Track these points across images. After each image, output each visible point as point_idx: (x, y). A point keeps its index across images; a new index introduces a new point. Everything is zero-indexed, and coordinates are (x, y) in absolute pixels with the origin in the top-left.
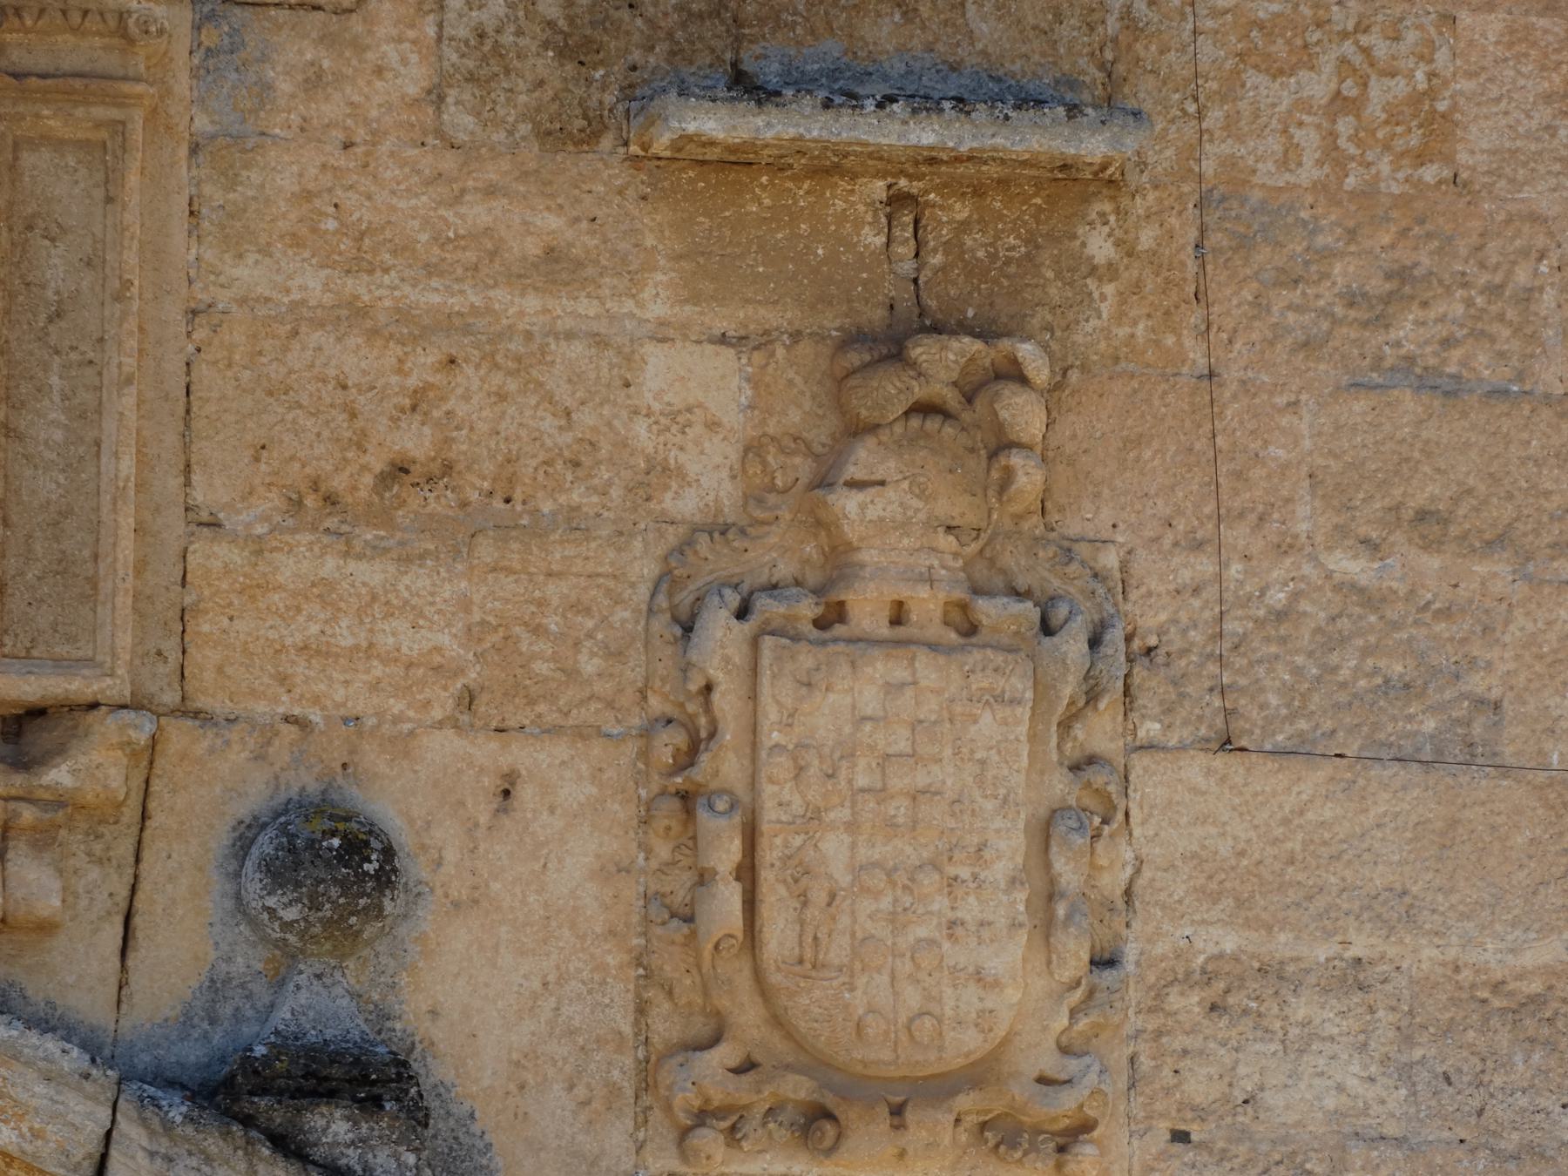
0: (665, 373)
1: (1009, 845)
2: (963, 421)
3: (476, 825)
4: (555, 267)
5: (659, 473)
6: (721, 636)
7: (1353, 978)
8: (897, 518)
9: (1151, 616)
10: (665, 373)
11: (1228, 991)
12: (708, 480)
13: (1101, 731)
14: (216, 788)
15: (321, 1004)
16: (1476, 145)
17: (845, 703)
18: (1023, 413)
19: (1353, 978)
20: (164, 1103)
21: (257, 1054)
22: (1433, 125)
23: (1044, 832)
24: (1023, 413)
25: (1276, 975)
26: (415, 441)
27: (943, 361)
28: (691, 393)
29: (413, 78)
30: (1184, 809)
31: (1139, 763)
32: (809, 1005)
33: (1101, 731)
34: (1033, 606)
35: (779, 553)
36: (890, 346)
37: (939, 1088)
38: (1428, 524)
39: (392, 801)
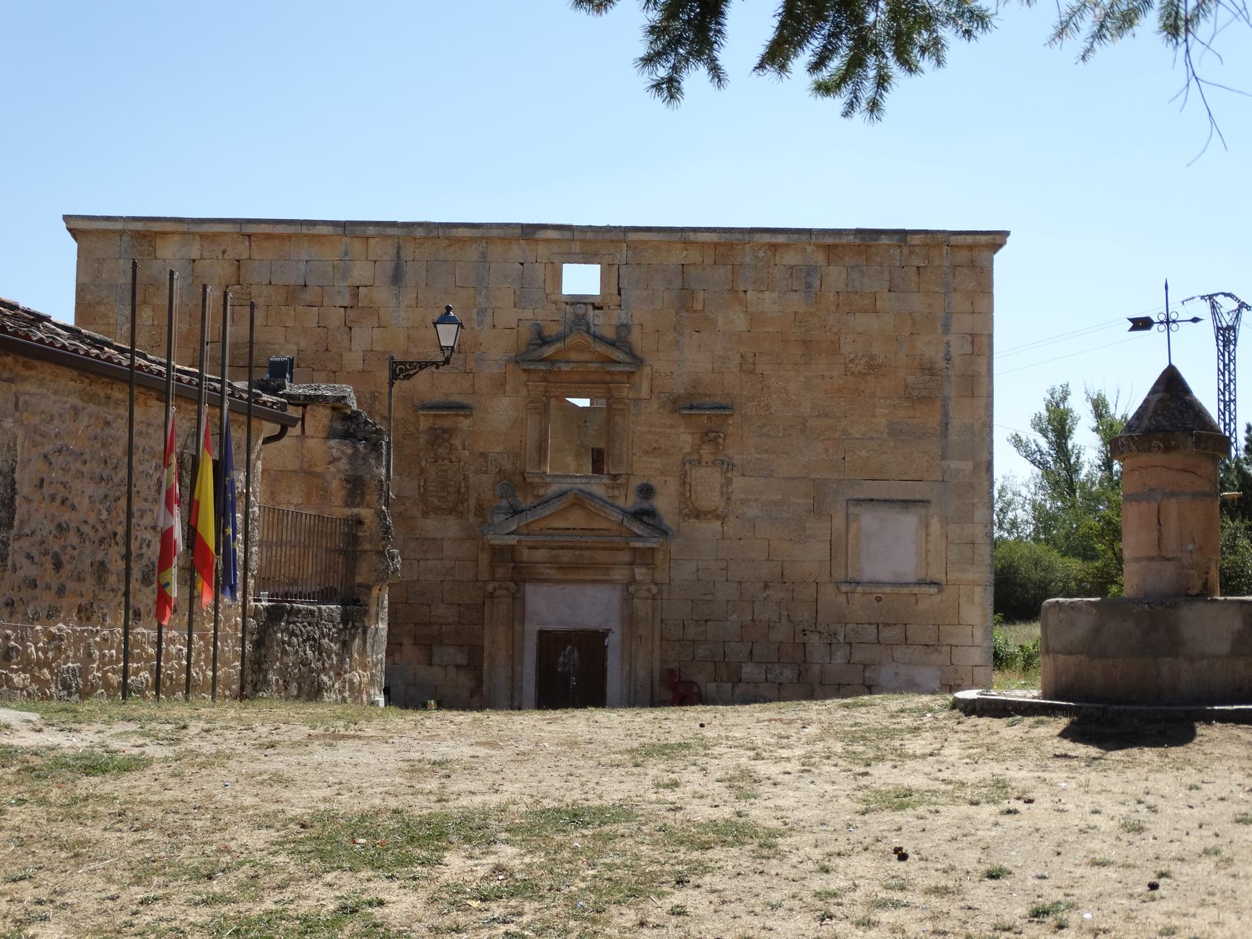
0: (683, 437)
1: (718, 487)
2: (714, 441)
3: (758, 757)
4: (672, 426)
5: (683, 447)
6: (687, 465)
7: (757, 500)
8: (706, 451)
9: (735, 462)
10: (683, 437)
11: (743, 502)
12: (688, 449)
13: (729, 475)
14: (636, 482)
15: (645, 505)
16: (773, 409)
18: (721, 441)
19: (757, 500)
21: (10, 420)
22: (768, 407)
23: (722, 486)
26: (656, 445)
27: (712, 435)
28: (685, 439)
29: (656, 406)
30: (738, 482)
31: (730, 267)
32: (696, 505)
33: (729, 475)
35: (695, 457)
36: (706, 434)
37: (710, 512)
38: (766, 451)
39: (653, 483)
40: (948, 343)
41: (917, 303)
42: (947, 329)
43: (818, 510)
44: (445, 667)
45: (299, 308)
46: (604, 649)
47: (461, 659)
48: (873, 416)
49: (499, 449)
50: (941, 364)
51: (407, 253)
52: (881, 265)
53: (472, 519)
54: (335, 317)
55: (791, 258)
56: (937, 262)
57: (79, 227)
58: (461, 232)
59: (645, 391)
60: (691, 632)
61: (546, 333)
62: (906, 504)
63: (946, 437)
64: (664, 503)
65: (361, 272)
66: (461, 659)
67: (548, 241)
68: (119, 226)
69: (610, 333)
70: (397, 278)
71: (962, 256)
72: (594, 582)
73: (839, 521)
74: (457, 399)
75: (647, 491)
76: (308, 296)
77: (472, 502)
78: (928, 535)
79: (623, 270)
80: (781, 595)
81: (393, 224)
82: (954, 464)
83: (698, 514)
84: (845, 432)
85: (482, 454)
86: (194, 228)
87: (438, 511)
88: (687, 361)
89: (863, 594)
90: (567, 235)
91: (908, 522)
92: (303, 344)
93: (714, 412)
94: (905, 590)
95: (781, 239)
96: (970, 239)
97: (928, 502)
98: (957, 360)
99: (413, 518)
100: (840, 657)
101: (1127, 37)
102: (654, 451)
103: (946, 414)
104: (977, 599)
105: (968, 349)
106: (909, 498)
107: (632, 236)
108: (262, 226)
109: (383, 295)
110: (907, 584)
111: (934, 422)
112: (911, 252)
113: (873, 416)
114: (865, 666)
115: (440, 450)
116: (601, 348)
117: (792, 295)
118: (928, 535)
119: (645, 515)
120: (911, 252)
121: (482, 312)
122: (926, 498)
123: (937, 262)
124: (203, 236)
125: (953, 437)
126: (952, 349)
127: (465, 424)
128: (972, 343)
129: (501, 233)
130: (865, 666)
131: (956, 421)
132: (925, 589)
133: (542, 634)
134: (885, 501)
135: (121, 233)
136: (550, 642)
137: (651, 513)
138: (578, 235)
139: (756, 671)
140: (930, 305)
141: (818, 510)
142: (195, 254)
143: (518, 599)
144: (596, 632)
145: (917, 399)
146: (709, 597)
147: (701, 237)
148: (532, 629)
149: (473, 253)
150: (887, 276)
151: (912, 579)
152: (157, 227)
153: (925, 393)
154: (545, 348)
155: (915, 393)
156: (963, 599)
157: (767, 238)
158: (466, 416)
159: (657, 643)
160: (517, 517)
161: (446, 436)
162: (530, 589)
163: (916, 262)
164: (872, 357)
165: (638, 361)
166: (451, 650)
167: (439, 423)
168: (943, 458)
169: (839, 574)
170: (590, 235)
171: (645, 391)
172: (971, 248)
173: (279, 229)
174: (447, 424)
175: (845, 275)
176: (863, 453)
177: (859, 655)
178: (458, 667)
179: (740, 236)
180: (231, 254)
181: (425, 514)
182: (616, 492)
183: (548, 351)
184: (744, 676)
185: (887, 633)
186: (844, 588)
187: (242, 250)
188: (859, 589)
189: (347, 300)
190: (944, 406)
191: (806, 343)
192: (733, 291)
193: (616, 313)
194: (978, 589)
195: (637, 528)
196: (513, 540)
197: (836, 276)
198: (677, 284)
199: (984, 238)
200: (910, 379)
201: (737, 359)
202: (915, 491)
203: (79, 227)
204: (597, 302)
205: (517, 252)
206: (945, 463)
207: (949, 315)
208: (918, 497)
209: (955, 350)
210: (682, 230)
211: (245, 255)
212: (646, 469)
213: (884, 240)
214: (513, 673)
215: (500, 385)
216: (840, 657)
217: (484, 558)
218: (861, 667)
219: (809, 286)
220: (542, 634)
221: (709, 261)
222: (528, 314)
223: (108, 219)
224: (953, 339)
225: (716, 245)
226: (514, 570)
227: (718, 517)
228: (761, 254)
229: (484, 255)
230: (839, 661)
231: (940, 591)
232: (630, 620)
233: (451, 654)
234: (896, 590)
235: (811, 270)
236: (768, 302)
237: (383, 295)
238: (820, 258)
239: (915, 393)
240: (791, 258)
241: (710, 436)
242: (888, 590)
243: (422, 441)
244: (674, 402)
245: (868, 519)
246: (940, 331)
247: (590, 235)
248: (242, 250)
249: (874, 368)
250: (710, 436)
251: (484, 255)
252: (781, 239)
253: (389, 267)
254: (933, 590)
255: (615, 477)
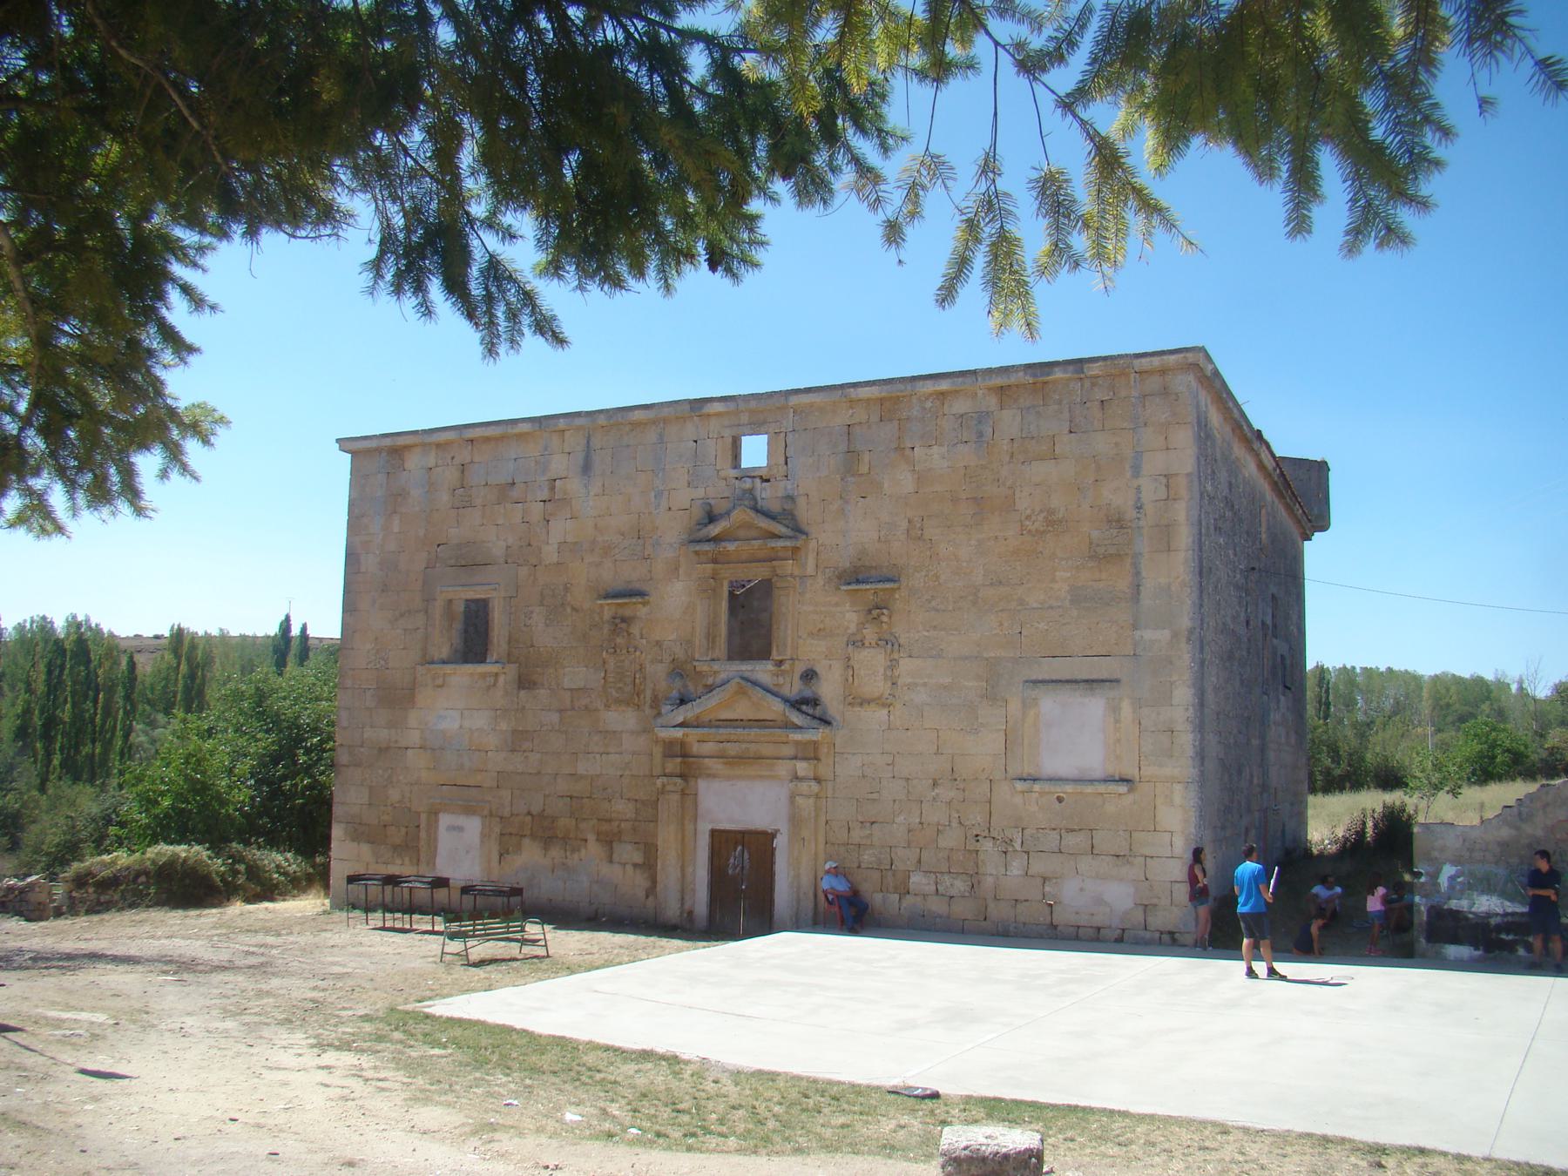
4: (837, 605)
8: (870, 633)
9: (902, 641)
11: (909, 687)
12: (853, 628)
13: (896, 656)
14: (800, 668)
15: (808, 693)
16: (943, 577)
17: (865, 654)
18: (885, 619)
19: (925, 684)
20: (748, 1092)
22: (937, 577)
24: (885, 619)
25: (916, 685)
28: (850, 617)
30: (906, 665)
31: (896, 423)
34: (888, 642)
36: (870, 611)
37: (873, 700)
38: (935, 628)
39: (817, 669)
40: (1138, 488)
41: (1102, 443)
42: (1137, 471)
43: (992, 696)
44: (624, 864)
45: (509, 506)
46: (773, 850)
47: (638, 857)
48: (1053, 580)
49: (673, 637)
50: (1131, 513)
51: (596, 442)
52: (1060, 402)
53: (648, 711)
54: (537, 509)
55: (960, 406)
56: (1123, 394)
57: (344, 444)
58: (638, 415)
59: (810, 570)
60: (857, 835)
61: (716, 511)
62: (1091, 683)
63: (1138, 601)
64: (829, 690)
65: (559, 464)
66: (638, 857)
67: (718, 415)
68: (374, 444)
69: (775, 507)
70: (586, 468)
71: (1154, 383)
72: (761, 777)
73: (1014, 706)
74: (637, 586)
75: (809, 676)
76: (515, 493)
77: (648, 693)
78: (1117, 721)
79: (790, 436)
80: (952, 794)
81: (578, 414)
82: (1148, 635)
83: (864, 702)
84: (1021, 602)
85: (657, 642)
86: (428, 439)
87: (618, 701)
88: (846, 531)
89: (1042, 794)
90: (732, 406)
91: (1094, 707)
92: (510, 541)
93: (880, 586)
94: (1089, 789)
95: (944, 386)
96: (1156, 361)
97: (1117, 681)
98: (1149, 508)
99: (596, 710)
100: (1016, 868)
101: (212, 403)
102: (819, 633)
103: (1138, 573)
104: (1177, 799)
105: (1162, 493)
106: (1094, 677)
107: (794, 400)
108: (860, 390)
109: (574, 485)
110: (1092, 781)
111: (1123, 585)
112: (1093, 385)
113: (1053, 580)
114: (1045, 879)
115: (619, 640)
116: (764, 523)
117: (961, 447)
118: (1117, 721)
119: (807, 704)
120: (1093, 385)
121: (659, 495)
122: (1114, 677)
123: (1123, 394)
124: (438, 445)
125: (1146, 601)
126: (1143, 495)
127: (642, 611)
128: (1167, 486)
129: (651, 414)
130: (1045, 879)
131: (1149, 585)
132: (1112, 787)
133: (713, 833)
134: (1068, 681)
135: (378, 450)
136: (722, 841)
137: (815, 702)
138: (742, 406)
139: (924, 881)
140: (1117, 444)
141: (992, 696)
142: (432, 463)
143: (688, 798)
144: (764, 833)
145: (1099, 557)
146: (875, 796)
147: (864, 393)
148: (704, 828)
149: (652, 436)
150: (1066, 415)
151: (1098, 774)
152: (401, 441)
153: (1112, 550)
154: (711, 527)
155: (1101, 550)
156: (1159, 801)
157: (930, 387)
158: (644, 604)
159: (821, 846)
160: (683, 708)
161: (624, 625)
162: (702, 785)
163: (1100, 394)
164: (1051, 512)
165: (798, 530)
166: (629, 847)
167: (620, 612)
168: (1135, 627)
169: (1014, 770)
170: (753, 404)
171: (810, 570)
172: (1163, 372)
173: (490, 432)
174: (628, 612)
175: (1019, 418)
176: (1042, 626)
177: (1038, 867)
178: (635, 865)
179: (901, 387)
180: (457, 461)
181: (607, 706)
182: (781, 680)
183: (715, 530)
184: (912, 887)
185: (1071, 840)
186: (1019, 786)
187: (464, 455)
188: (1037, 787)
189: (545, 495)
190: (1135, 565)
191: (977, 501)
192: (899, 449)
193: (782, 484)
194: (1178, 788)
195: (796, 718)
196: (678, 733)
197: (1009, 421)
198: (843, 447)
199: (1172, 358)
200: (1095, 534)
201: (905, 524)
202: (1103, 668)
203: (344, 444)
204: (764, 473)
205: (690, 430)
206: (1138, 633)
207: (1138, 455)
208: (1105, 676)
209: (1147, 496)
210: (842, 386)
211: (468, 459)
212: (812, 651)
213: (1058, 374)
214: (683, 876)
215: (674, 570)
216: (1016, 868)
217: (658, 751)
218: (1039, 881)
219: (980, 434)
220: (713, 833)
221: (875, 418)
222: (700, 493)
223: (808, 390)
224: (1146, 484)
225: (882, 401)
226: (684, 765)
227: (884, 705)
228: (928, 405)
229: (661, 436)
230: (1016, 872)
231: (1130, 791)
232: (795, 820)
233: (629, 853)
234: (1079, 788)
235: (983, 416)
236: (935, 458)
237: (574, 485)
238: (992, 402)
239: (1101, 550)
240: (960, 406)
241: (876, 611)
242: (1069, 788)
243: (605, 631)
244: (839, 577)
245: (1049, 704)
246: (1129, 474)
247: (753, 404)
248: (464, 455)
249: (1054, 523)
250: (876, 611)
251: (661, 436)
252: (944, 386)
253: (580, 456)
254: (1123, 789)
255: (780, 663)
